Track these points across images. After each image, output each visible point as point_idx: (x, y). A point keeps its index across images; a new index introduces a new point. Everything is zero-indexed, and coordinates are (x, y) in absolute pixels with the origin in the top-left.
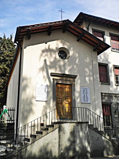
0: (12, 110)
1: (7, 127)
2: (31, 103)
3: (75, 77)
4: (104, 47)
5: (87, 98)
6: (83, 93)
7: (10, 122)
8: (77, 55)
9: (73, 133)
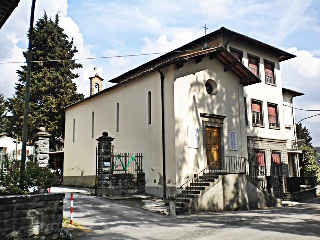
0: (139, 157)
1: (138, 178)
2: (184, 151)
3: (222, 118)
4: (253, 80)
5: (234, 145)
6: (231, 138)
7: (117, 173)
8: (224, 90)
9: (236, 185)
